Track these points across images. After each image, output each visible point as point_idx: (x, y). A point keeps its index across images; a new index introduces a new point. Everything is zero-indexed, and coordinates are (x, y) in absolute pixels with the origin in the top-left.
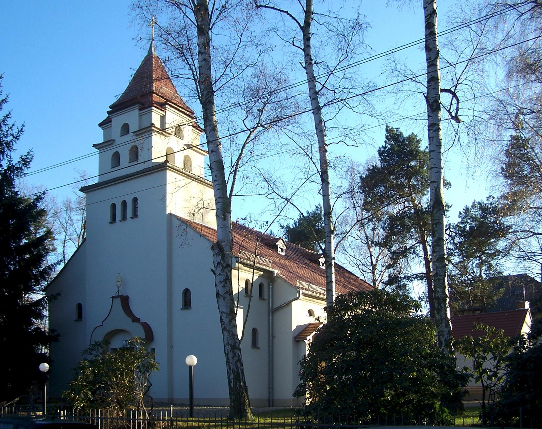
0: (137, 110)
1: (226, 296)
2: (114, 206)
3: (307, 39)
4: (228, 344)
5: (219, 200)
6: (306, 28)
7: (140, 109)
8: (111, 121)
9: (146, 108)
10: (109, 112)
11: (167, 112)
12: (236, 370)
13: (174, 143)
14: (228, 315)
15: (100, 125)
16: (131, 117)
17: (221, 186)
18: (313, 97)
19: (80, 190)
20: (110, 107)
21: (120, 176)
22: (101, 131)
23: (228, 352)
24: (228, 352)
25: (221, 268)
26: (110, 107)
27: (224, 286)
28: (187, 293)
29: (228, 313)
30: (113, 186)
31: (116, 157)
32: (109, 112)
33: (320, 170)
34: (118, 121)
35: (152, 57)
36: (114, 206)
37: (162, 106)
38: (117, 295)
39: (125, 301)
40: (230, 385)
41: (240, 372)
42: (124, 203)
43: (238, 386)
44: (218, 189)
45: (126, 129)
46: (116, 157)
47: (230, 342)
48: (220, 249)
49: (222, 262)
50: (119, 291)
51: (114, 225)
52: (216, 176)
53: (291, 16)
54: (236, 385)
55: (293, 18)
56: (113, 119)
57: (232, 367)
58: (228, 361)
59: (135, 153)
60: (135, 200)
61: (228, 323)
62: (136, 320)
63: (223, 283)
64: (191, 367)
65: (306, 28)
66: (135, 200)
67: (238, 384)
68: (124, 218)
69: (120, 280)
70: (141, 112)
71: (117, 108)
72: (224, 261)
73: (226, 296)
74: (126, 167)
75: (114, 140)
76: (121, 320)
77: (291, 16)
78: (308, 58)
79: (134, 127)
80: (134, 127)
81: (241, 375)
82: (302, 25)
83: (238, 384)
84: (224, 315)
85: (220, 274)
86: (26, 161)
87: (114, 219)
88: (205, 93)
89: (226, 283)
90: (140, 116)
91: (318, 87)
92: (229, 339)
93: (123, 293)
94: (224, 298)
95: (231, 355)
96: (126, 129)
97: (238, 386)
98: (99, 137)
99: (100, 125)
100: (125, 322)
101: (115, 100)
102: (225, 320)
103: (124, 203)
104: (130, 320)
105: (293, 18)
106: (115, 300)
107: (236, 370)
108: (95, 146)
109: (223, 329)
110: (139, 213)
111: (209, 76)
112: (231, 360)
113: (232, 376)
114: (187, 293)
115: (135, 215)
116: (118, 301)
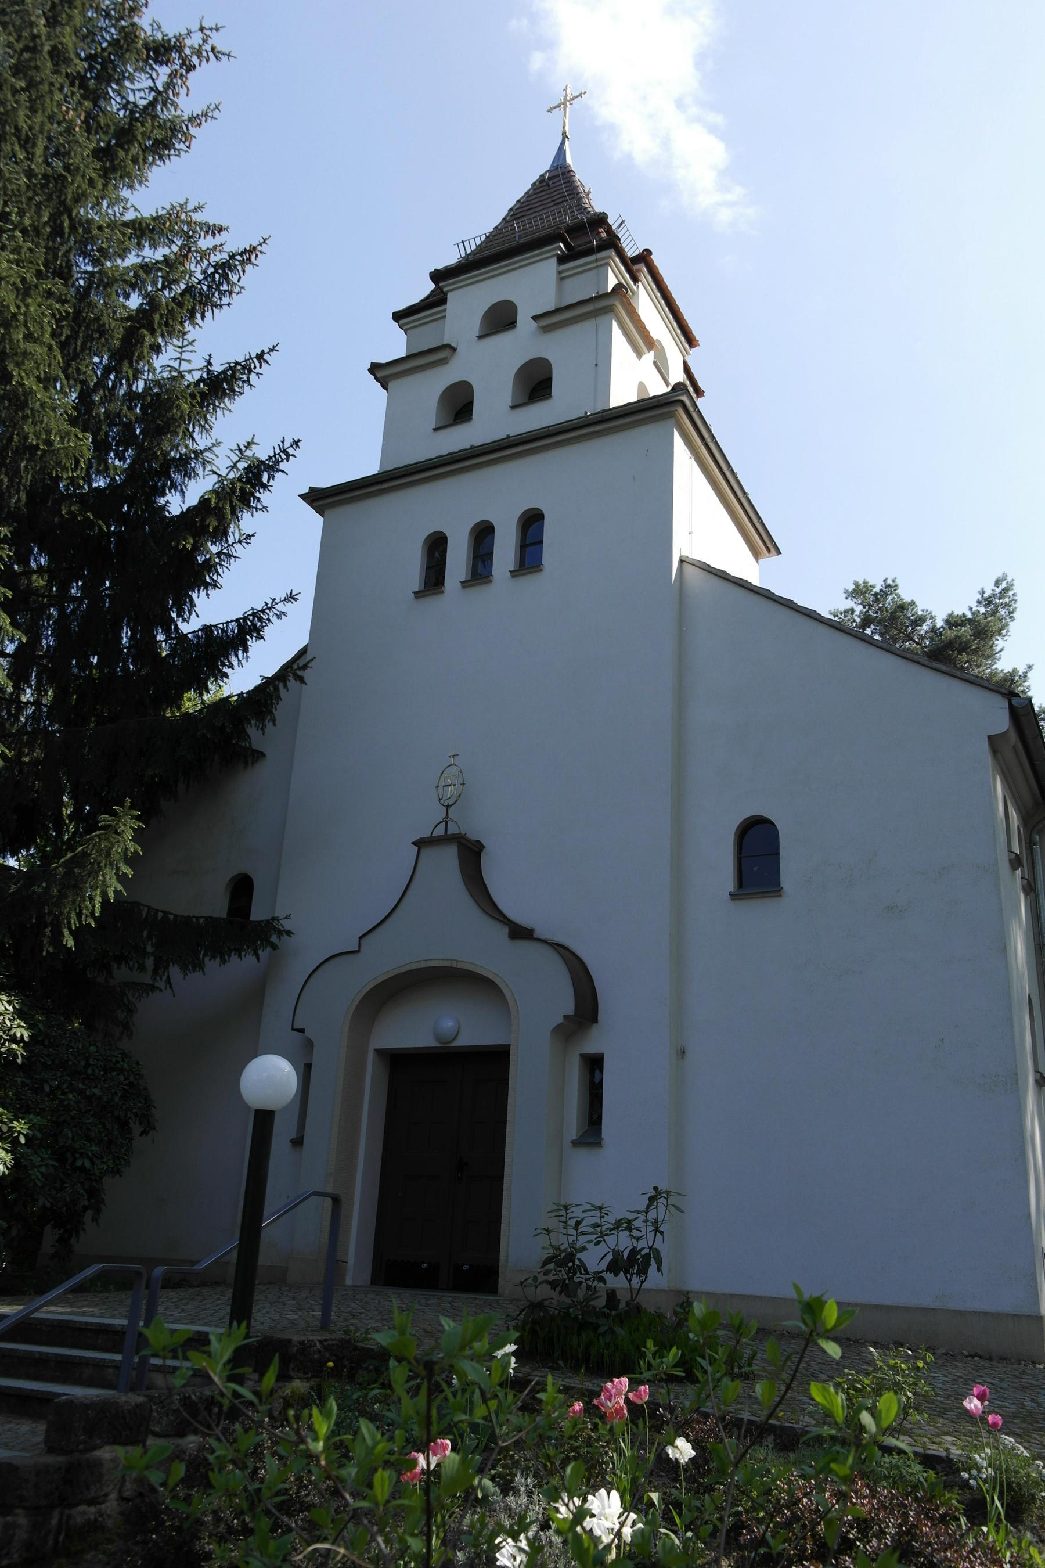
7: (562, 260)
8: (443, 301)
15: (398, 316)
16: (534, 285)
31: (459, 406)
38: (440, 831)
39: (471, 854)
46: (459, 406)
50: (446, 820)
51: (434, 604)
56: (450, 296)
59: (535, 383)
60: (532, 522)
62: (519, 933)
70: (563, 267)
74: (495, 417)
87: (434, 578)
96: (500, 319)
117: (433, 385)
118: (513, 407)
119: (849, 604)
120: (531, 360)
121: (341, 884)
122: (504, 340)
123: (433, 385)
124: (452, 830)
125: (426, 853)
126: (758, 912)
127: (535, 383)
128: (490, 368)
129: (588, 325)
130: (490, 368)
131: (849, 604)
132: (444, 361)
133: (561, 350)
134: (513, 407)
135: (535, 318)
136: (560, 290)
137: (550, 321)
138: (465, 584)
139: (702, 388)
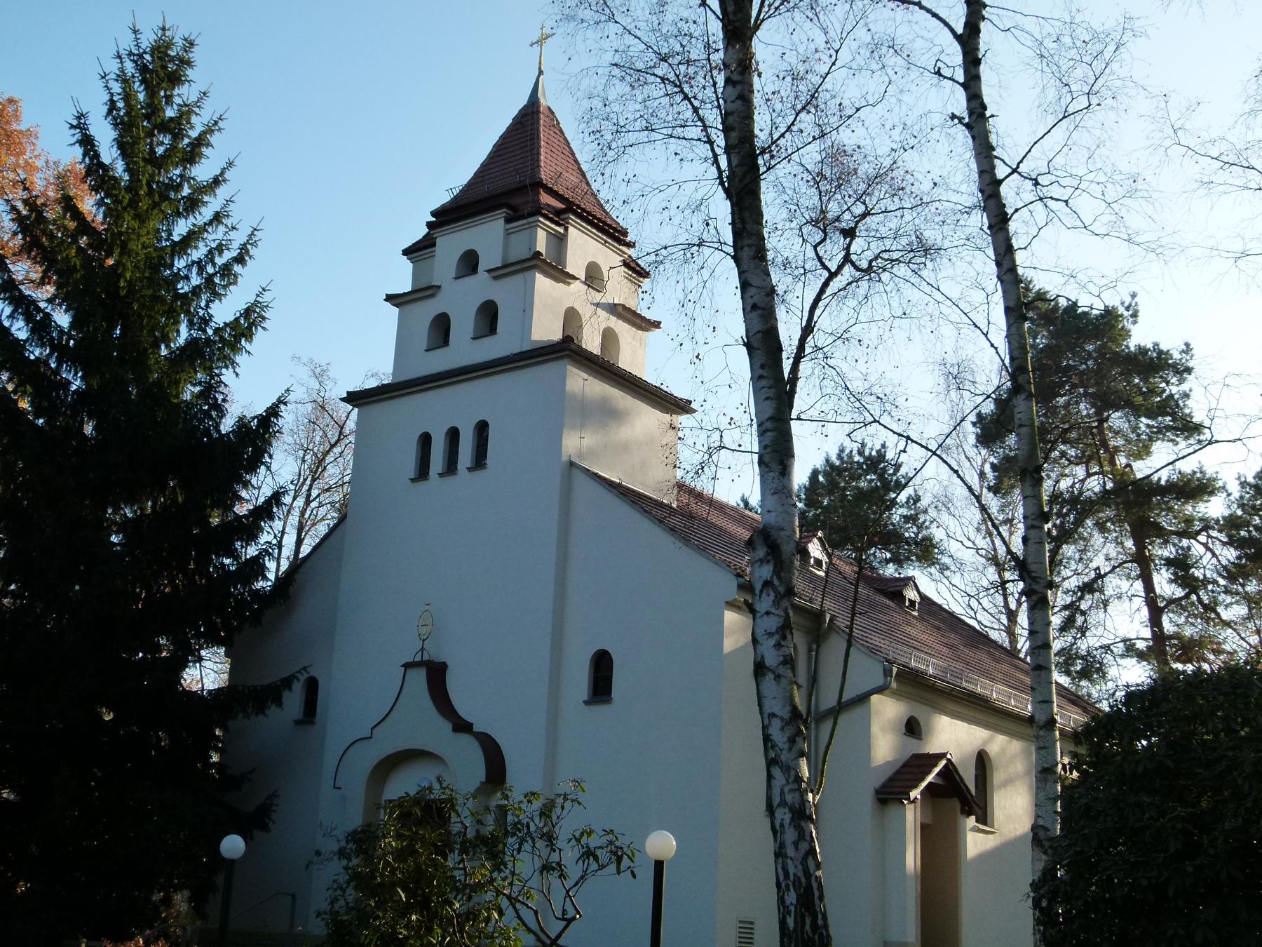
0: (502, 221)
1: (781, 670)
2: (426, 440)
3: (972, 61)
4: (783, 803)
5: (768, 425)
6: (969, 39)
7: (508, 220)
8: (434, 245)
9: (523, 217)
10: (429, 225)
11: (571, 229)
12: (803, 880)
13: (576, 294)
14: (787, 724)
15: (406, 252)
16: (488, 237)
17: (773, 390)
18: (988, 190)
19: (342, 400)
20: (434, 214)
21: (434, 371)
22: (407, 266)
23: (782, 825)
24: (782, 825)
25: (772, 597)
26: (434, 214)
27: (778, 646)
28: (602, 665)
29: (787, 716)
30: (424, 394)
31: (441, 329)
32: (429, 225)
33: (1007, 361)
34: (452, 245)
35: (538, 112)
36: (426, 440)
37: (559, 217)
38: (418, 659)
39: (436, 674)
40: (783, 923)
41: (815, 885)
42: (453, 434)
43: (808, 927)
44: (767, 398)
45: (469, 263)
46: (441, 329)
47: (789, 798)
48: (769, 547)
49: (776, 582)
50: (422, 649)
51: (422, 486)
52: (762, 367)
53: (928, 11)
54: (804, 923)
55: (935, 15)
56: (438, 241)
57: (792, 870)
58: (780, 854)
59: (488, 317)
60: (482, 428)
61: (786, 746)
62: (462, 726)
63: (777, 637)
64: (659, 865)
65: (969, 39)
66: (482, 428)
67: (808, 921)
68: (451, 467)
69: (429, 622)
70: (509, 226)
71: (446, 217)
72: (779, 578)
73: (781, 670)
74: (465, 348)
75: (439, 287)
76: (420, 725)
77: (928, 11)
78: (975, 104)
79: (489, 260)
80: (489, 260)
81: (817, 894)
82: (960, 30)
83: (808, 921)
84: (776, 724)
85: (768, 613)
86: (247, 324)
87: (423, 471)
88: (739, 171)
89: (784, 638)
90: (508, 234)
91: (1001, 171)
92: (786, 789)
93: (435, 653)
94: (778, 677)
95: (790, 835)
96: (469, 263)
97: (808, 927)
98: (402, 278)
99: (406, 252)
100: (429, 729)
101: (446, 198)
102: (779, 737)
103: (453, 434)
104: (447, 726)
105: (935, 15)
106: (410, 672)
107: (803, 880)
108: (389, 298)
109: (771, 763)
110: (490, 460)
111: (749, 137)
112: (790, 851)
113: (791, 898)
114: (602, 665)
115: (480, 459)
116: (420, 676)
117: (426, 312)
118: (474, 339)
119: (1185, 387)
120: (431, 694)
121: (364, 692)
122: (470, 281)
123: (426, 312)
124: (426, 658)
125: (409, 671)
126: (601, 709)
127: (488, 317)
128: (461, 299)
129: (519, 277)
130: (461, 299)
131: (1185, 387)
132: (432, 296)
133: (502, 293)
134: (474, 339)
135: (489, 271)
136: (506, 245)
137: (499, 273)
138: (441, 475)
139: (488, 461)
